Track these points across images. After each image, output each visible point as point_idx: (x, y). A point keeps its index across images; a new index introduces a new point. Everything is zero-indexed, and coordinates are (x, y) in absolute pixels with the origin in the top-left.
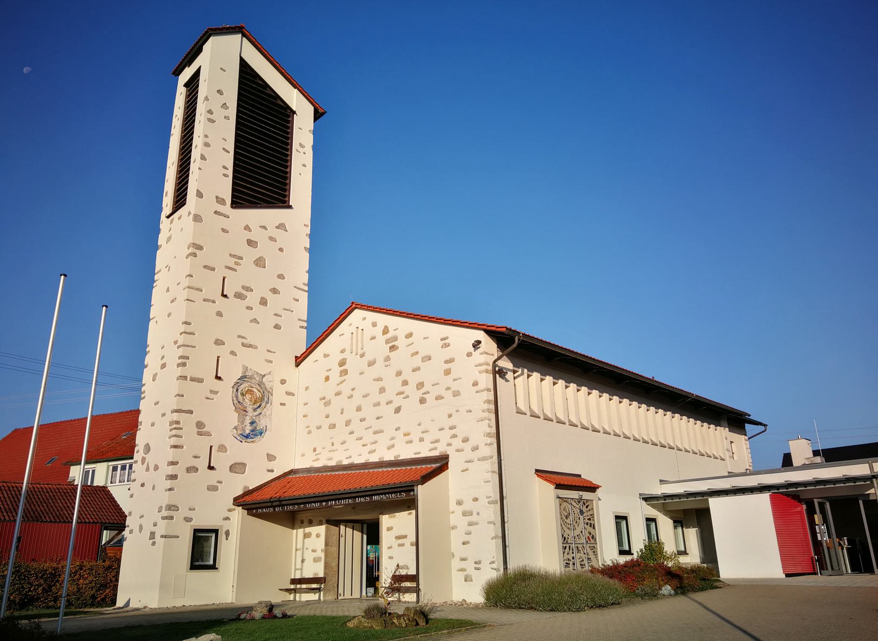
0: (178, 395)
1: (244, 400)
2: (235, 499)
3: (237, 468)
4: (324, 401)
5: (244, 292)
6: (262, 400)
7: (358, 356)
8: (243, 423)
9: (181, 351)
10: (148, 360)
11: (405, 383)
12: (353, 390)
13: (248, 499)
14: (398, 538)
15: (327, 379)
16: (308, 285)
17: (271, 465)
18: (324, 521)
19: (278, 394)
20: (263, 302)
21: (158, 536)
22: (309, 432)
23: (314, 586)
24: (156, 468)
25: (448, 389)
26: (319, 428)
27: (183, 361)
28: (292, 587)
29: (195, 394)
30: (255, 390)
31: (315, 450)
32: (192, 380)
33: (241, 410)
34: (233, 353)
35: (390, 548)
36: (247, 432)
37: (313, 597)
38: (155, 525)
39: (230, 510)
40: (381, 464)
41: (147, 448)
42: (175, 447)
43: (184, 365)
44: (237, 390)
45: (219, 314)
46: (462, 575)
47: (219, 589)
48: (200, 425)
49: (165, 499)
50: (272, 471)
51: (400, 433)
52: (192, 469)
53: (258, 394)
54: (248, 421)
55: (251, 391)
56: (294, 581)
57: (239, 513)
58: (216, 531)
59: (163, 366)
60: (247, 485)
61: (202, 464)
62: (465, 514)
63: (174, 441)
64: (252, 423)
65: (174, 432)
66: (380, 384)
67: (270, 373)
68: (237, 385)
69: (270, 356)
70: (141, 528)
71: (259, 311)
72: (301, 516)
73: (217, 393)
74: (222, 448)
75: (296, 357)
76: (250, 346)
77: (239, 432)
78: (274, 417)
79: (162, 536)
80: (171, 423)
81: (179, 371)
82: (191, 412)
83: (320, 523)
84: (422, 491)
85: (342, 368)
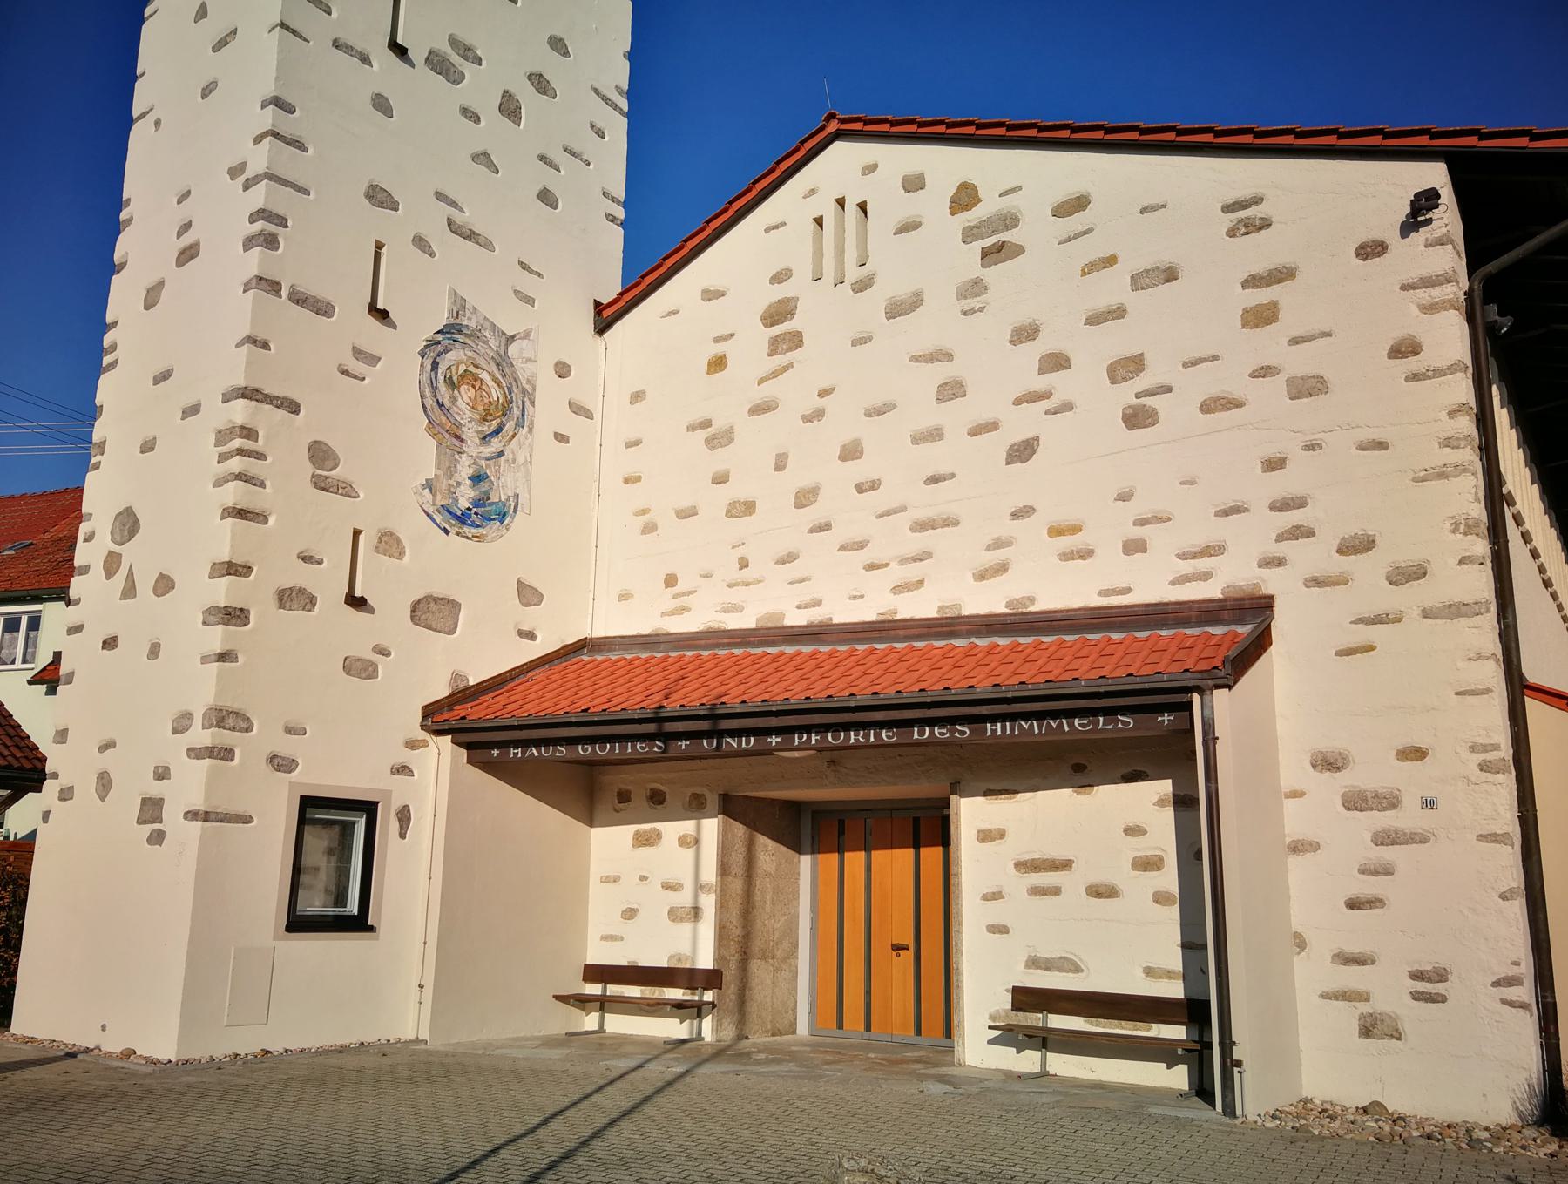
0: (252, 340)
1: (454, 400)
2: (429, 711)
3: (434, 612)
4: (703, 434)
5: (456, 59)
6: (505, 416)
7: (847, 286)
8: (450, 473)
9: (258, 197)
10: (123, 247)
11: (1056, 362)
12: (823, 393)
13: (476, 712)
14: (1027, 866)
15: (718, 364)
16: (631, 95)
17: (531, 617)
18: (713, 800)
19: (548, 410)
20: (510, 108)
21: (172, 818)
22: (650, 528)
23: (676, 994)
24: (164, 585)
25: (1264, 372)
26: (686, 514)
27: (268, 231)
28: (594, 989)
29: (307, 352)
30: (484, 375)
31: (671, 581)
32: (299, 299)
33: (448, 434)
34: (420, 242)
35: (995, 896)
36: (464, 503)
37: (674, 1028)
38: (162, 774)
39: (412, 745)
40: (948, 626)
41: (128, 524)
42: (242, 514)
43: (270, 242)
44: (435, 365)
45: (382, 104)
46: (1347, 1016)
47: (383, 992)
48: (320, 454)
49: (202, 689)
50: (531, 636)
51: (1034, 528)
52: (294, 598)
53: (495, 392)
54: (465, 471)
55: (476, 378)
56: (595, 973)
57: (442, 754)
58: (369, 809)
59: (188, 254)
60: (462, 668)
61: (329, 584)
62: (1356, 802)
63: (233, 494)
64: (477, 479)
65: (236, 464)
66: (942, 372)
67: (527, 335)
68: (434, 349)
69: (527, 283)
70: (104, 783)
71: (493, 131)
72: (617, 779)
73: (373, 360)
74: (389, 543)
75: (597, 304)
76: (471, 236)
77: (441, 501)
78: (534, 468)
79: (192, 815)
80: (222, 436)
81: (254, 262)
82: (294, 408)
83: (696, 807)
84: (1225, 709)
85: (777, 330)
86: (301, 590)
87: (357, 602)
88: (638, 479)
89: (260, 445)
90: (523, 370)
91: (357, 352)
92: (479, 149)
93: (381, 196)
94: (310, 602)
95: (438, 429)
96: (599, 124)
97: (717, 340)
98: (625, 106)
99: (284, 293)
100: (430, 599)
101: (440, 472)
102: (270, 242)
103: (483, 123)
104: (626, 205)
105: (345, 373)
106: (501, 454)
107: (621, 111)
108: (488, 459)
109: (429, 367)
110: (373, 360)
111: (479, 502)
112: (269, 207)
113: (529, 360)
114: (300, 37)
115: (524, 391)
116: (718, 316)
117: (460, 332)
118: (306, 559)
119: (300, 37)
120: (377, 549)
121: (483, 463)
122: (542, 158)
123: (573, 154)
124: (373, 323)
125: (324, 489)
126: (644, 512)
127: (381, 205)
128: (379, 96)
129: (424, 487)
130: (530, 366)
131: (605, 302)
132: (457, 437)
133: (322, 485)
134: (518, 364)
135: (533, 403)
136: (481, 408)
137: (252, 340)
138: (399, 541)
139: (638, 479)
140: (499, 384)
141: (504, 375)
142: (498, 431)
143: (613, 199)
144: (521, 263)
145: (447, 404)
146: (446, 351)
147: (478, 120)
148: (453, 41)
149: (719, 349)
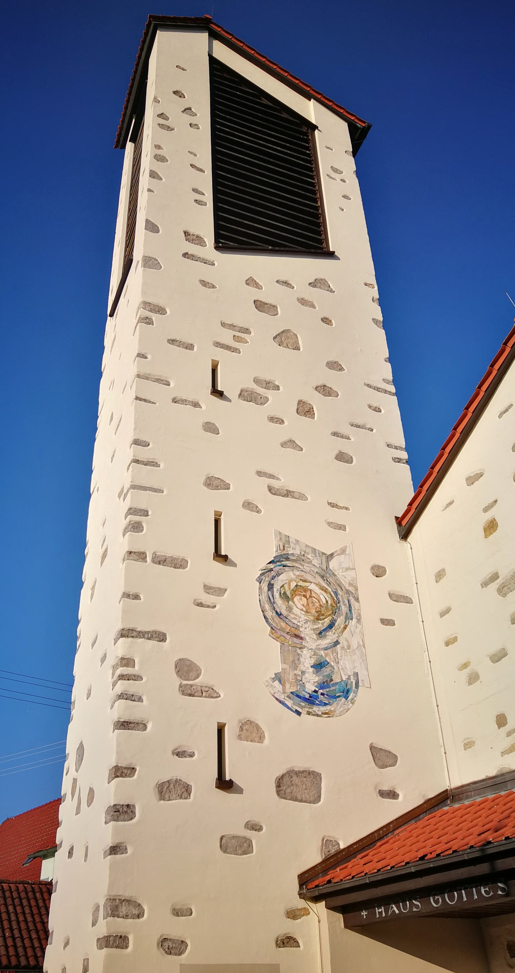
0: (126, 595)
1: (290, 609)
2: (305, 879)
5: (260, 390)
8: (295, 665)
13: (340, 875)
16: (395, 382)
17: (389, 778)
19: (372, 601)
22: (473, 678)
30: (312, 587)
36: (310, 688)
39: (293, 914)
43: (136, 527)
44: (271, 587)
45: (211, 428)
48: (185, 668)
50: (392, 795)
52: (172, 789)
53: (323, 597)
54: (307, 661)
55: (305, 589)
57: (319, 923)
64: (319, 666)
67: (343, 551)
68: (268, 576)
69: (337, 516)
74: (251, 730)
75: (397, 518)
76: (288, 494)
77: (290, 689)
82: (161, 637)
86: (178, 782)
87: (224, 784)
88: (455, 639)
89: (136, 670)
90: (345, 578)
91: (208, 589)
92: (286, 439)
93: (215, 483)
94: (185, 790)
95: (279, 633)
96: (375, 404)
97: (486, 510)
98: (393, 389)
99: (149, 559)
100: (291, 773)
101: (285, 666)
102: (136, 527)
103: (286, 423)
104: (407, 449)
105: (200, 605)
106: (337, 643)
107: (390, 393)
108: (326, 649)
109: (266, 589)
110: (221, 592)
111: (323, 685)
112: (134, 506)
113: (348, 569)
114: (150, 402)
115: (348, 592)
116: (483, 491)
117: (287, 559)
118: (180, 754)
119: (150, 402)
120: (240, 737)
121: (322, 653)
122: (335, 434)
123: (358, 426)
124: (218, 566)
125: (190, 695)
126: (465, 665)
127: (217, 488)
128: (207, 423)
129: (274, 680)
130: (351, 573)
131: (400, 515)
132: (297, 636)
133: (188, 692)
134: (340, 574)
135: (357, 600)
136: (313, 611)
137: (126, 595)
138: (258, 728)
139: (455, 639)
140: (326, 591)
141: (329, 584)
142: (331, 626)
143: (396, 448)
144: (330, 504)
145: (284, 612)
146: (278, 575)
147: (282, 422)
148: (257, 381)
149: (488, 516)
